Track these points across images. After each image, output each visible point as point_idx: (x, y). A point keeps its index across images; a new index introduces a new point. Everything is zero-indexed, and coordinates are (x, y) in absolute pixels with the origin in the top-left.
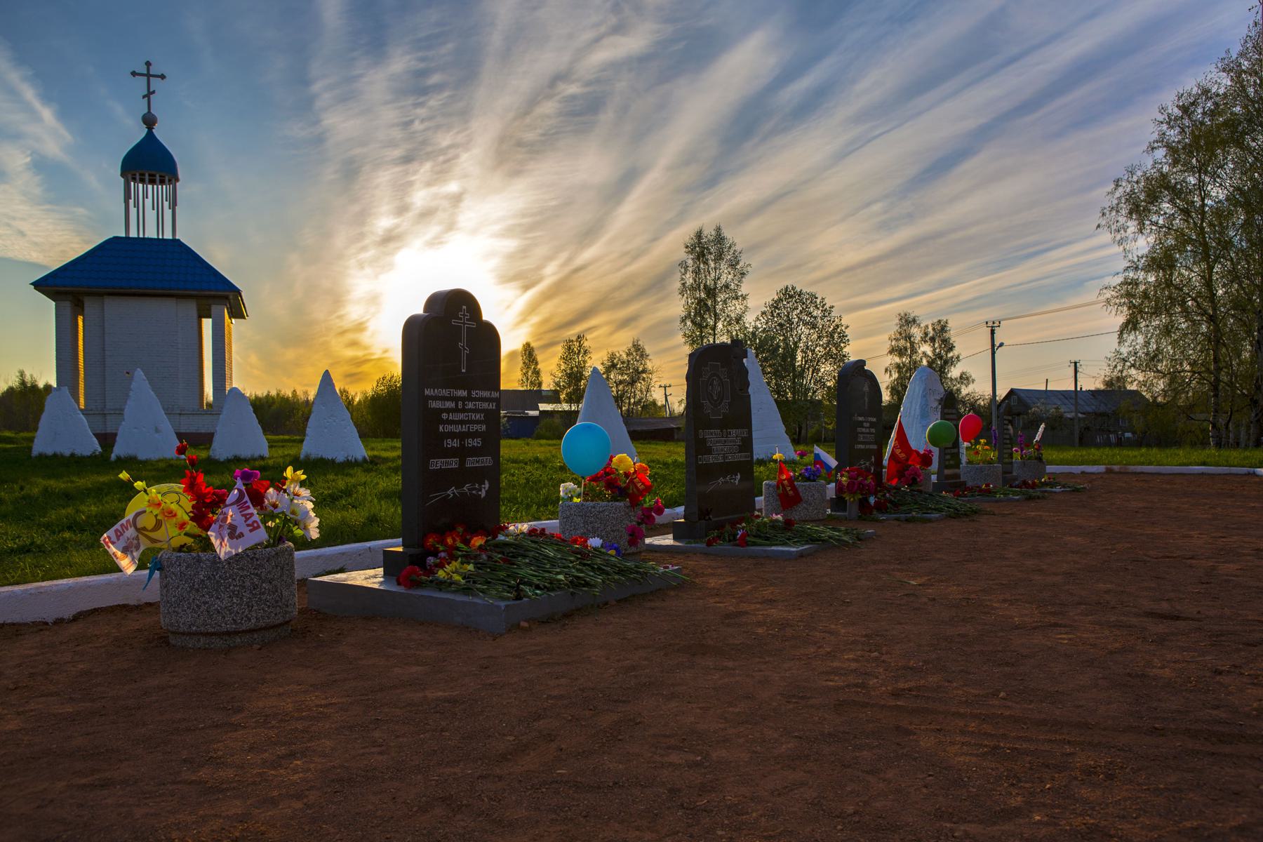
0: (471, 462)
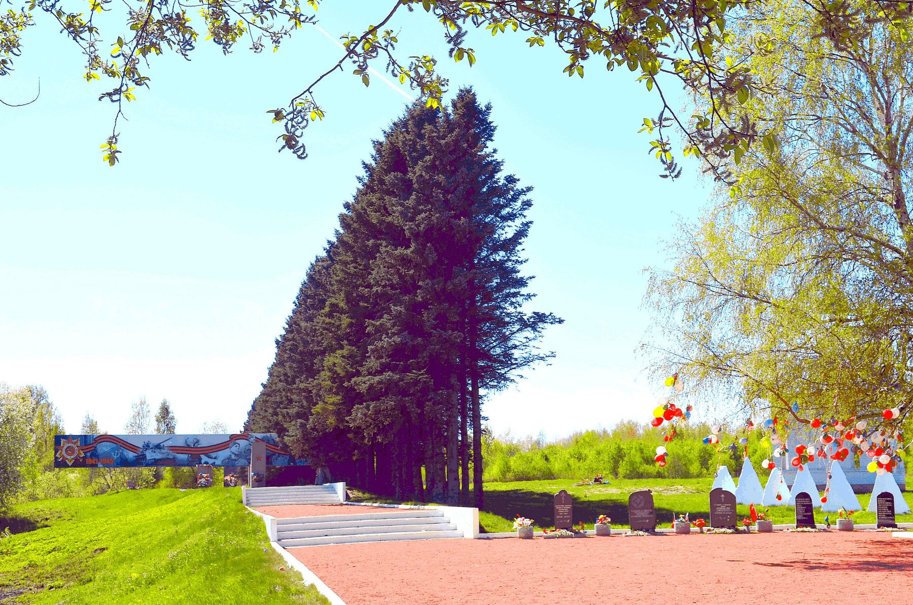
0: (565, 517)
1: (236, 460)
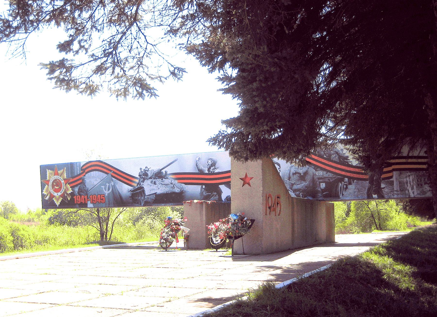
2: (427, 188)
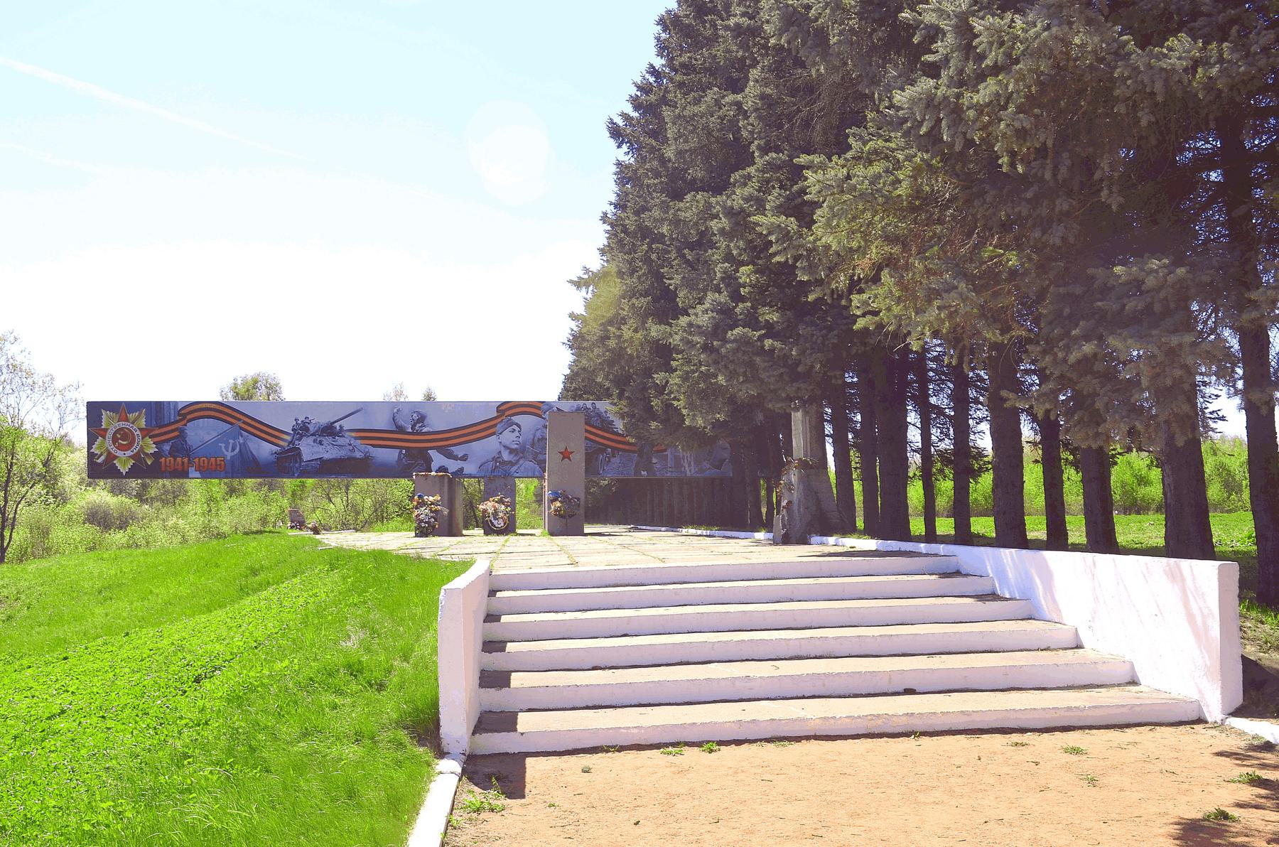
1: (512, 464)
2: (706, 465)
